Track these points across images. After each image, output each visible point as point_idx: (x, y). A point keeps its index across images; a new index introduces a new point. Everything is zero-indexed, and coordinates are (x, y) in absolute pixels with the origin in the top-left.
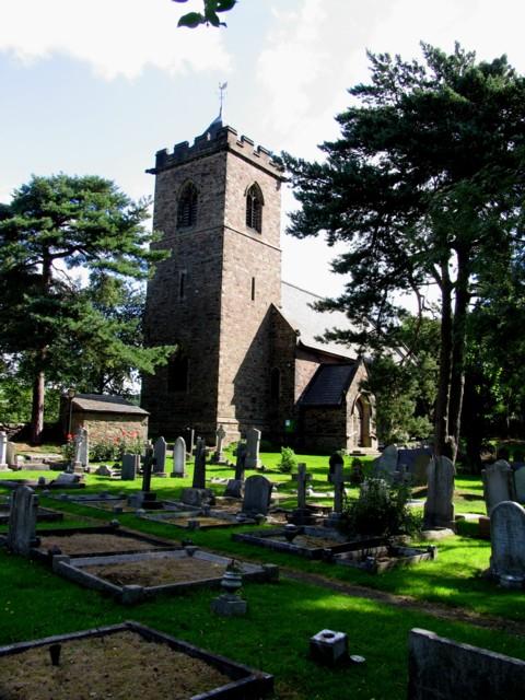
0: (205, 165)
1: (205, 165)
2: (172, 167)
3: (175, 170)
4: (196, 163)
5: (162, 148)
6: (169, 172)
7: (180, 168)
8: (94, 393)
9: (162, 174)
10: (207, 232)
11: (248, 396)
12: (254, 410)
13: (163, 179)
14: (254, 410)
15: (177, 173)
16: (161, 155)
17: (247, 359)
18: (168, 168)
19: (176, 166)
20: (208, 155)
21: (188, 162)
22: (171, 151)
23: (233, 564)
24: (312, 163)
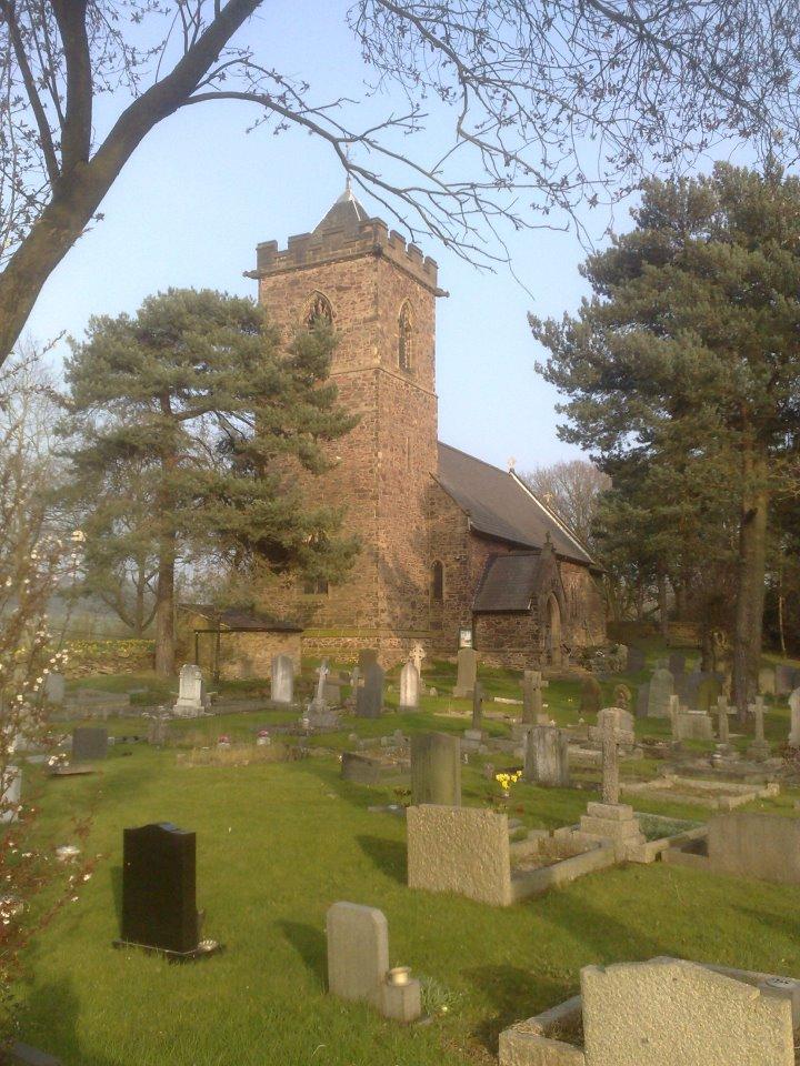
0: (343, 275)
1: (343, 275)
2: (284, 271)
3: (291, 276)
4: (327, 270)
5: (271, 239)
6: (282, 277)
7: (299, 274)
8: (738, 598)
9: (270, 282)
10: (351, 375)
11: (408, 600)
12: (414, 619)
13: (273, 289)
14: (414, 619)
15: (295, 283)
16: (266, 251)
17: (193, 880)
18: (278, 273)
19: (293, 270)
20: (347, 259)
21: (315, 265)
22: (283, 246)
23: (262, 475)
24: (437, 392)
